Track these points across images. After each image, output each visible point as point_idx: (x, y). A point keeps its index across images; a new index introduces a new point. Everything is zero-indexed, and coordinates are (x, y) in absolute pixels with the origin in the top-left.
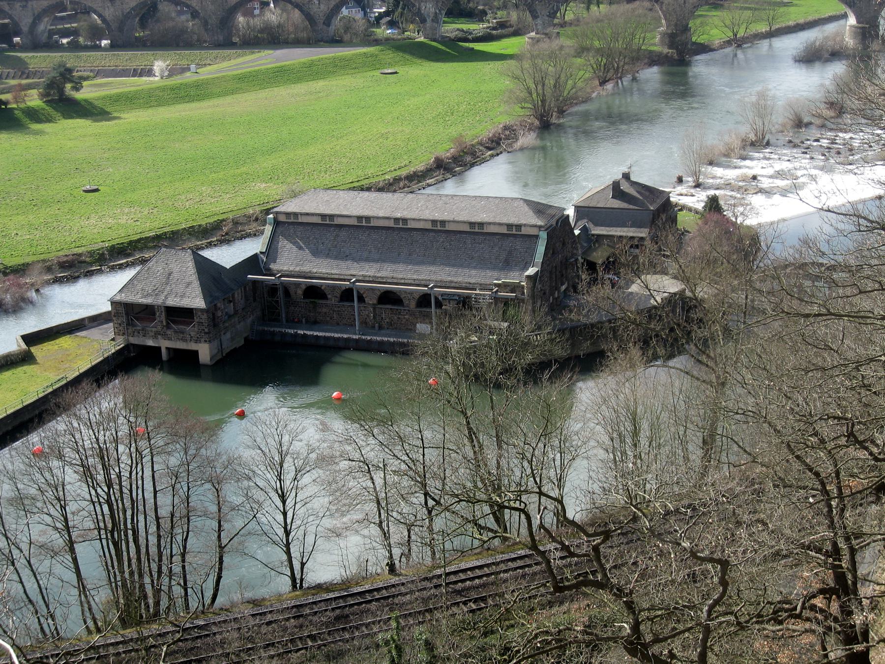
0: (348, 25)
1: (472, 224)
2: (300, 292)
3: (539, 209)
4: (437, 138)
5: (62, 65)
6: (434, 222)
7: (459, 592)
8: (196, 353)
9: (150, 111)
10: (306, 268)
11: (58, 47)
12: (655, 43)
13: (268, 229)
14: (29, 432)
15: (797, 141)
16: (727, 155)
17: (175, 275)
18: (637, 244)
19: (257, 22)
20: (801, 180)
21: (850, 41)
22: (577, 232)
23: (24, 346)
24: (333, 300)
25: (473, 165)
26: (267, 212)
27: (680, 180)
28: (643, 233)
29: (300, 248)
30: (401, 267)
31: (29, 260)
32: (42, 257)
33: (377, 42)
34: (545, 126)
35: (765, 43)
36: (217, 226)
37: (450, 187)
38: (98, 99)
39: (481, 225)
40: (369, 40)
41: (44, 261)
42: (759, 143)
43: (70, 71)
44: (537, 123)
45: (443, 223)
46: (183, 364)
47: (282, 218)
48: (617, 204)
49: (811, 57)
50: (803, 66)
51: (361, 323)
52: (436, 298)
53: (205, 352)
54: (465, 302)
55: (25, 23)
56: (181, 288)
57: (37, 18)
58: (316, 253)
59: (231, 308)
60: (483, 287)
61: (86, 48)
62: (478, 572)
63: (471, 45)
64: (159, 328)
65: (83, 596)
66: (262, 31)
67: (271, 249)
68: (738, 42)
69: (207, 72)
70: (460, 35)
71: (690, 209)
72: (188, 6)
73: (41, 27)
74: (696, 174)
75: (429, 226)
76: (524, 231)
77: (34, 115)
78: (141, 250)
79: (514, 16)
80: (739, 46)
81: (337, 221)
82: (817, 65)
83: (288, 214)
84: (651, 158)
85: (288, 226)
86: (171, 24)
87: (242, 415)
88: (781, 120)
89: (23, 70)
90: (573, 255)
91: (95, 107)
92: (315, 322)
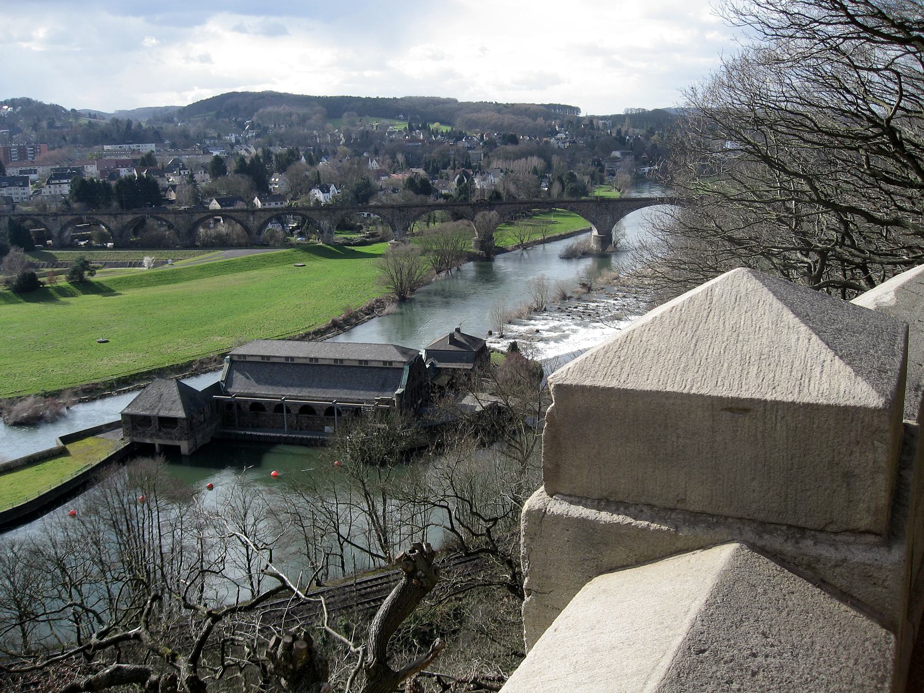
0: (273, 234)
1: (360, 361)
2: (247, 406)
3: (404, 351)
4: (333, 308)
5: (82, 259)
6: (336, 360)
7: (362, 596)
8: (179, 447)
9: (142, 290)
10: (252, 391)
11: (79, 248)
12: (471, 246)
13: (226, 366)
14: (65, 502)
15: (564, 308)
16: (520, 318)
17: (165, 395)
18: (468, 373)
19: (212, 232)
20: (567, 332)
21: (594, 246)
22: (427, 366)
23: (61, 444)
24: (269, 412)
25: (356, 325)
26: (224, 355)
27: (490, 333)
28: (469, 366)
29: (248, 378)
30: (314, 390)
31: (61, 387)
32: (71, 386)
33: (291, 246)
34: (402, 300)
35: (541, 247)
36: (189, 365)
37: (342, 338)
38: (107, 281)
39: (366, 362)
40: (286, 244)
41: (72, 388)
42: (539, 310)
43: (87, 262)
44: (397, 297)
45: (341, 360)
46: (172, 455)
47: (235, 358)
48: (453, 348)
49: (570, 256)
50: (566, 262)
51: (288, 426)
52: (338, 410)
53: (185, 447)
54: (357, 411)
55: (55, 232)
56: (169, 405)
57: (64, 228)
58: (259, 381)
59: (202, 418)
60: (368, 401)
61: (97, 248)
62: (375, 583)
63: (353, 248)
64: (154, 431)
65: (380, 513)
66: (215, 238)
67: (229, 379)
68: (524, 246)
69: (179, 265)
70: (346, 241)
71: (498, 351)
72: (166, 221)
73: (67, 234)
74: (500, 329)
75: (332, 363)
76: (394, 365)
77: (63, 292)
78: (138, 381)
79: (380, 229)
80: (525, 249)
81: (272, 360)
82: (574, 260)
83: (239, 356)
84: (472, 319)
85: (239, 364)
86: (155, 233)
87: (211, 487)
88: (553, 295)
89: (53, 262)
90: (425, 381)
91: (104, 287)
92: (258, 426)
